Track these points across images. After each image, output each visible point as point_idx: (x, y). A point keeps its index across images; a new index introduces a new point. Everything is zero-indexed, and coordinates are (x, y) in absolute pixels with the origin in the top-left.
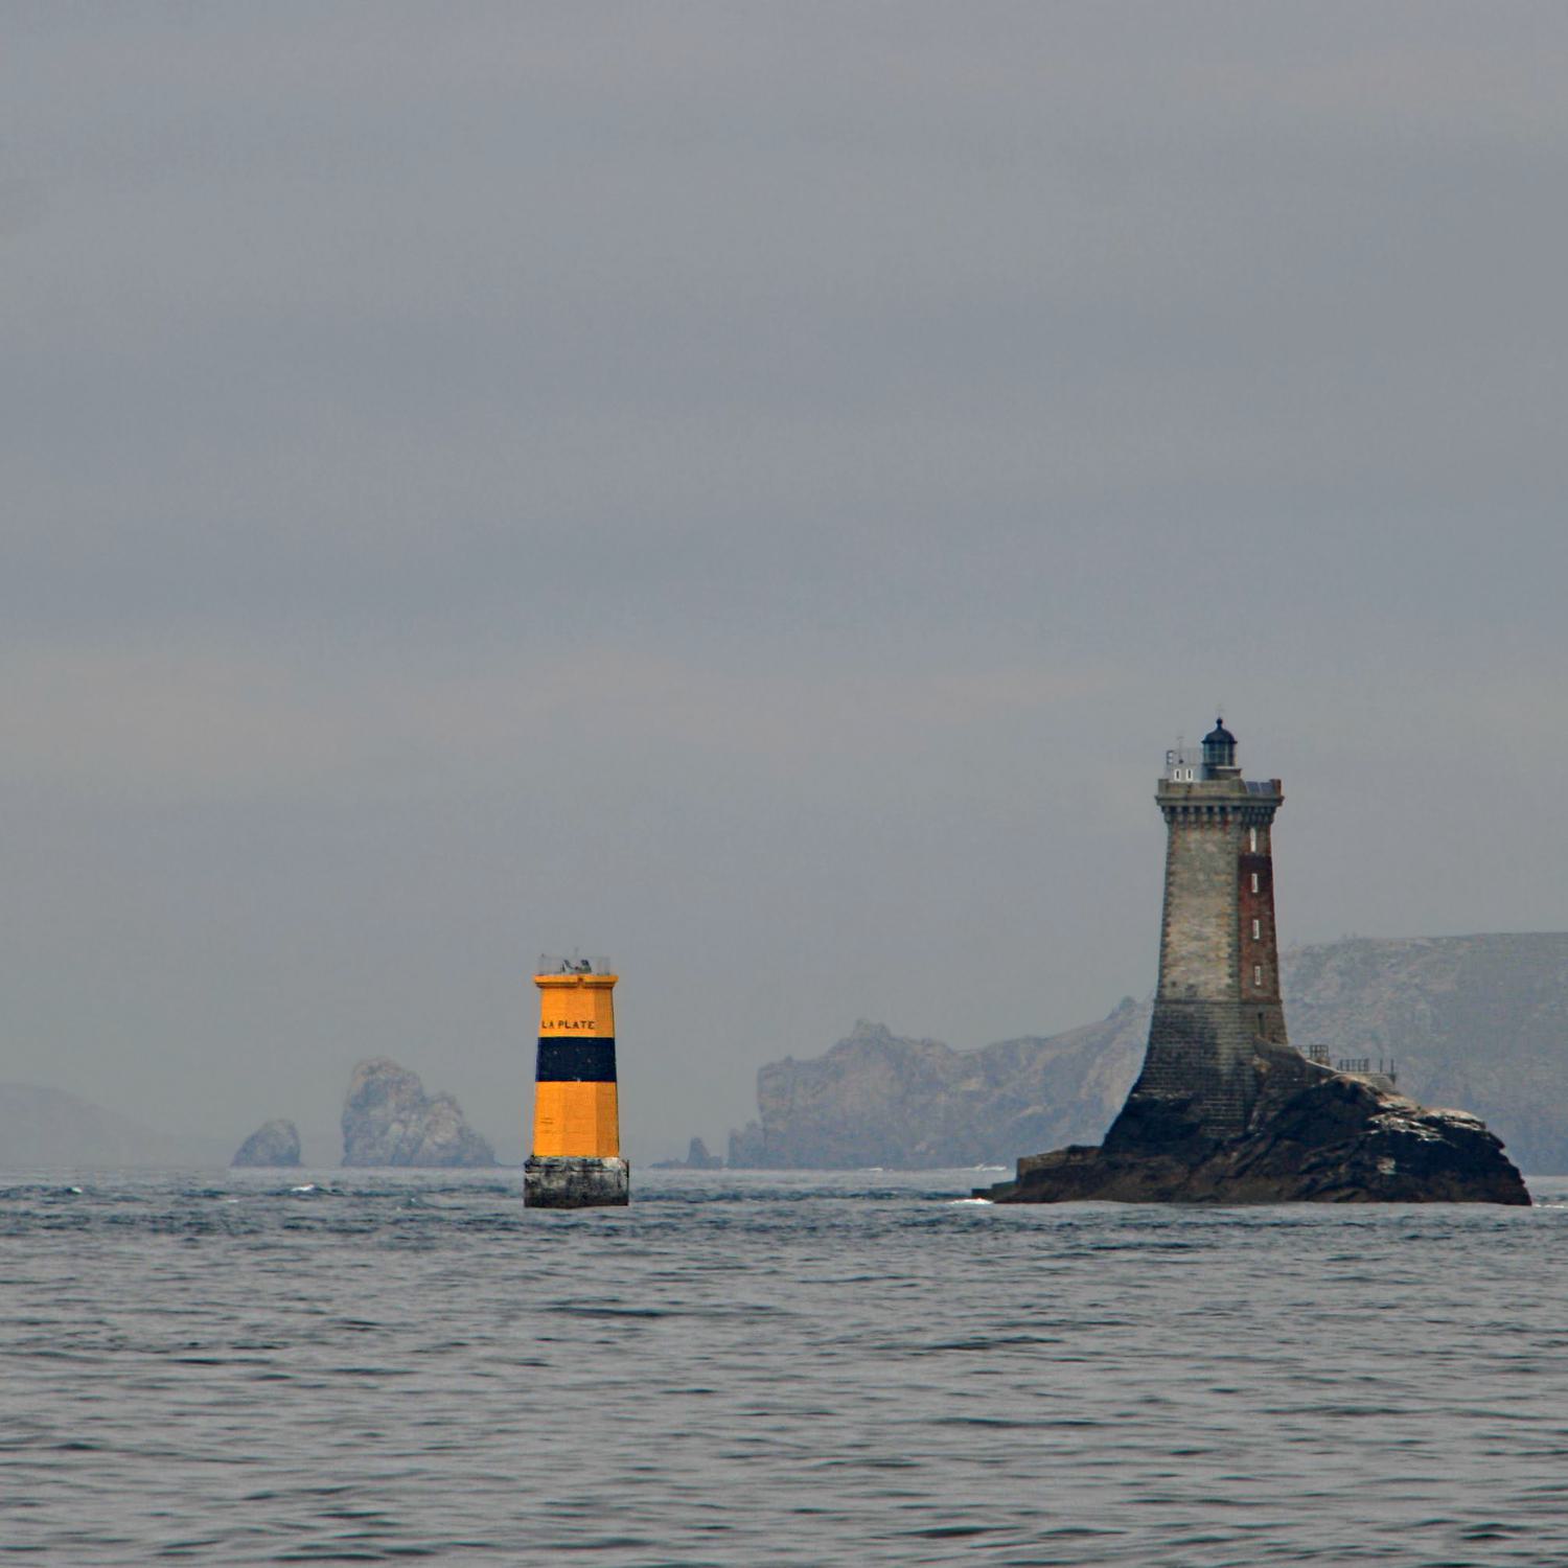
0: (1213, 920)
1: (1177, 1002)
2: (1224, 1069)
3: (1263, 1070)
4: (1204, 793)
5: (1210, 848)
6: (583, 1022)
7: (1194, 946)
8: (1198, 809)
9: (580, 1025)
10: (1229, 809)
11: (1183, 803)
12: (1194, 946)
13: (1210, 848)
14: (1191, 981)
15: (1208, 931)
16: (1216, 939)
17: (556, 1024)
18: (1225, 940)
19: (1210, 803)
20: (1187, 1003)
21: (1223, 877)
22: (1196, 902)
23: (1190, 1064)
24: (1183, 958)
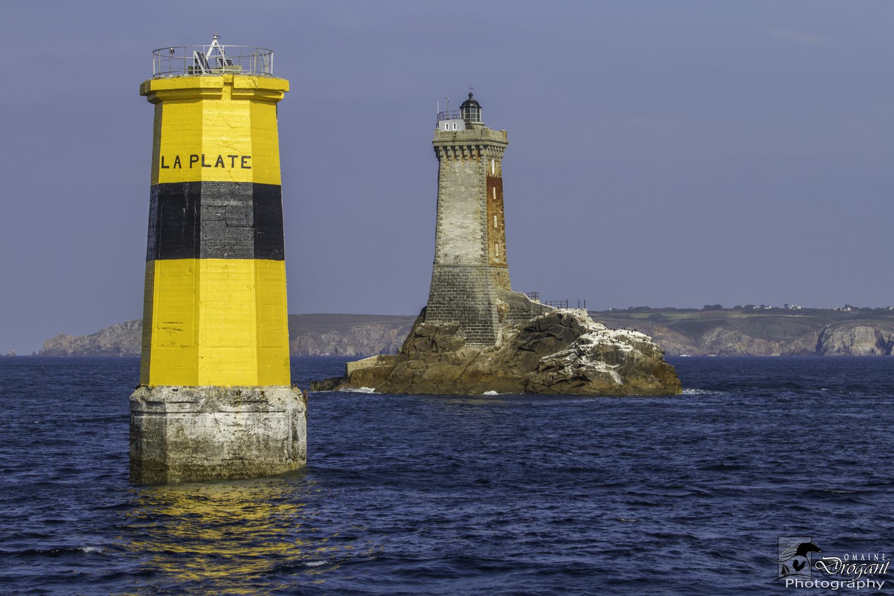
0: (470, 216)
1: (448, 266)
2: (480, 307)
3: (503, 308)
4: (465, 137)
5: (468, 171)
6: (233, 157)
7: (459, 232)
8: (461, 147)
9: (227, 161)
10: (481, 147)
11: (452, 144)
12: (459, 232)
13: (468, 171)
14: (457, 254)
15: (468, 222)
16: (472, 226)
17: (185, 162)
18: (479, 227)
19: (469, 143)
20: (454, 267)
21: (477, 189)
22: (458, 205)
23: (457, 304)
24: (452, 239)
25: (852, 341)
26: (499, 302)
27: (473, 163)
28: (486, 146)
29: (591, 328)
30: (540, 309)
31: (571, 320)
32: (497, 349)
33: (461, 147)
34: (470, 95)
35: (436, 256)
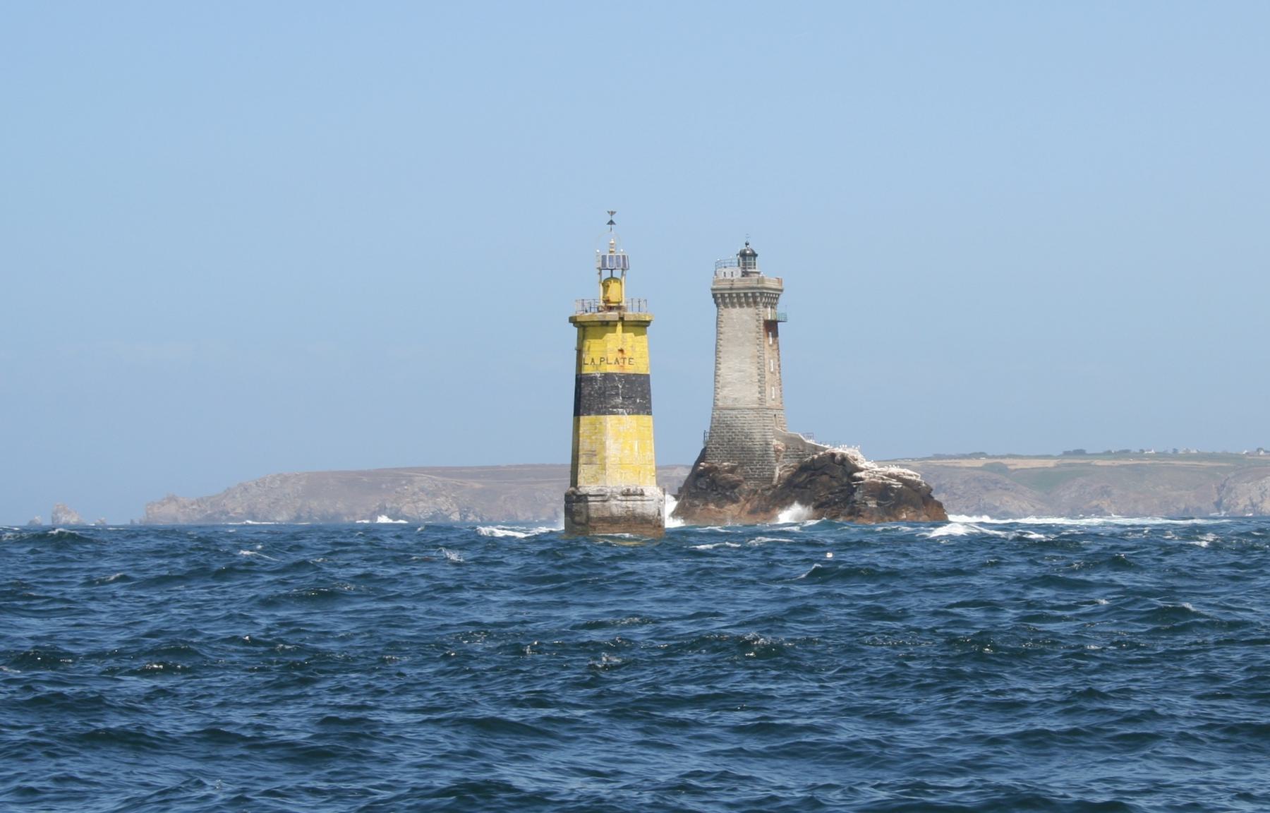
2: (757, 447)
5: (746, 317)
25: (1263, 495)
26: (775, 442)
27: (751, 310)
28: (762, 294)
29: (862, 466)
30: (816, 449)
31: (844, 459)
32: (775, 487)
33: (738, 295)
34: (747, 257)
35: (715, 399)
